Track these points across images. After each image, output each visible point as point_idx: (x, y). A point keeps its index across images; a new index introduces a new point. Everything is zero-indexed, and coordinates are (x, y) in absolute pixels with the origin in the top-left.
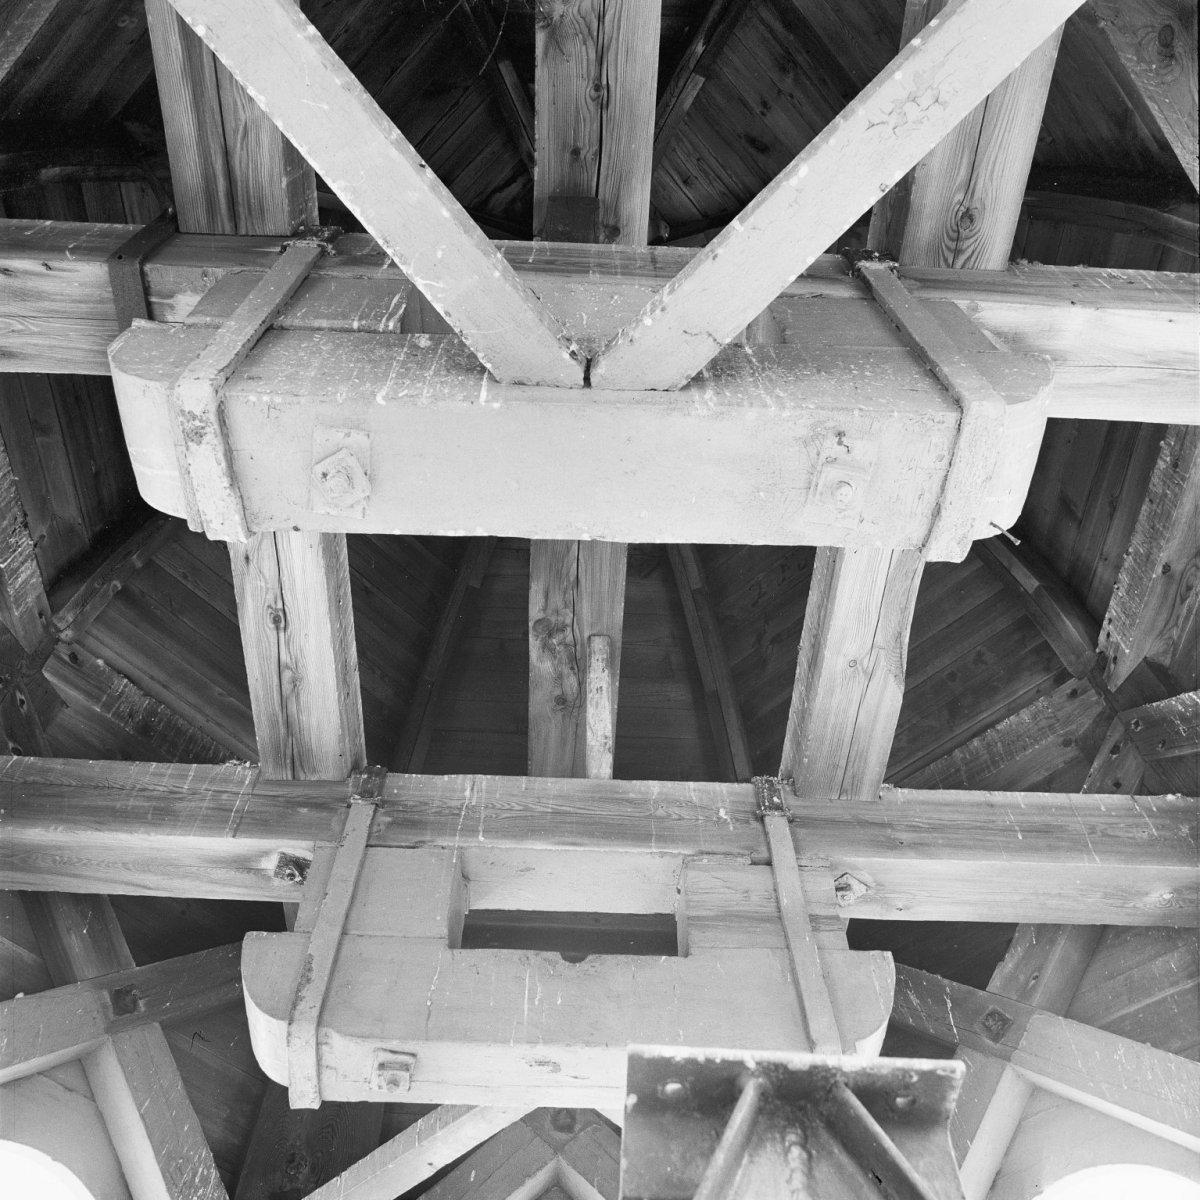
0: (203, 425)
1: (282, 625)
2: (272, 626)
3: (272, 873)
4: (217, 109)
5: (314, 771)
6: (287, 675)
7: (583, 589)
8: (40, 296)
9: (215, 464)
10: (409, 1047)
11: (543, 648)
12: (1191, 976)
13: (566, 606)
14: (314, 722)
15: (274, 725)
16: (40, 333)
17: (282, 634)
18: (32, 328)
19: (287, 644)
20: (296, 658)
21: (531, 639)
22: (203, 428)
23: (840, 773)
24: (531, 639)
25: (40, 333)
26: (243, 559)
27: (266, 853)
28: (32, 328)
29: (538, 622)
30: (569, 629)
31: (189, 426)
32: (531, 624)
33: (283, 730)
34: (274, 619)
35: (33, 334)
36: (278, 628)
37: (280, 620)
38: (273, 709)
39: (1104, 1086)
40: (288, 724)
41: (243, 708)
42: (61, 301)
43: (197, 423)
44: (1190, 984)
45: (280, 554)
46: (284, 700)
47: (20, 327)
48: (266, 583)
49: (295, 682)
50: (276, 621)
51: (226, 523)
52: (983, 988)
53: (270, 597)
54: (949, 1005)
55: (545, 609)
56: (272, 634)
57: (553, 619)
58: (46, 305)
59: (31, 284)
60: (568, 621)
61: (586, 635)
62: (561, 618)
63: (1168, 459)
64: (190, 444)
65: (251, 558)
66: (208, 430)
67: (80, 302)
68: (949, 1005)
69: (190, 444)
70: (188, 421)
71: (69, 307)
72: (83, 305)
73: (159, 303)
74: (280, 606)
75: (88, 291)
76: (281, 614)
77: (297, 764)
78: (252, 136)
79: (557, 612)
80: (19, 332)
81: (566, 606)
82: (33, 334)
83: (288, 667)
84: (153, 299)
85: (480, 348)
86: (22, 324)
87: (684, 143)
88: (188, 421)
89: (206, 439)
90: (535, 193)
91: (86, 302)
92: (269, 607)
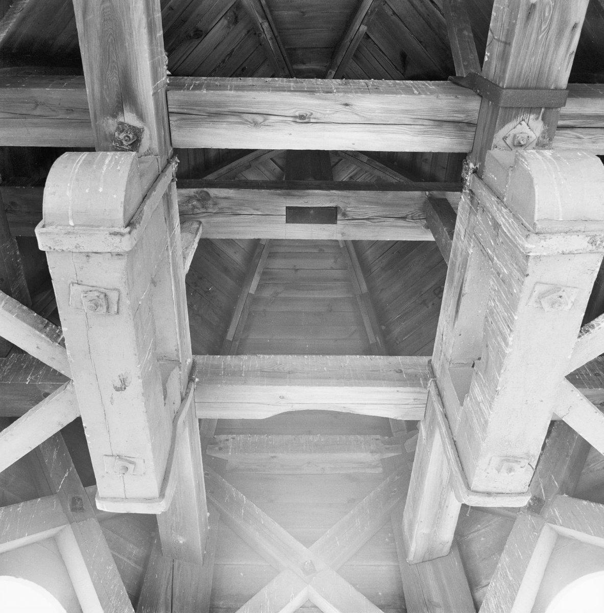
0: (597, 244)
1: (298, 120)
2: (297, 114)
3: (121, 119)
4: (591, 126)
5: (179, 127)
6: (259, 119)
7: (232, 218)
8: (558, 45)
9: (576, 249)
10: (124, 309)
11: (189, 197)
12: (136, 562)
13: (219, 209)
14: (222, 131)
15: (217, 104)
16: (537, 39)
17: (291, 119)
18: (541, 36)
19: (282, 121)
20: (273, 126)
21: (195, 190)
22: (595, 245)
23: (213, 401)
24: (194, 189)
25: (537, 39)
26: (347, 102)
27: (141, 116)
28: (541, 36)
29: (208, 194)
30: (204, 210)
31: (598, 238)
32: (205, 189)
33: (214, 110)
34: (303, 116)
35: (538, 35)
36: (295, 117)
37: (303, 119)
38: (230, 106)
39: (95, 573)
40: (218, 114)
41: (422, 244)
42: (552, 57)
43: (599, 242)
44: (133, 565)
45: (349, 125)
46: (239, 114)
47: (543, 29)
48: (328, 114)
49: (256, 124)
50: (302, 117)
51: (543, 249)
52: (84, 486)
53: (318, 115)
54: (66, 475)
55: (217, 197)
56: (291, 112)
57: (210, 202)
58: (553, 45)
59: (565, 42)
60: (210, 210)
61: (202, 220)
62: (211, 206)
63: (315, 441)
64: (589, 238)
65: (347, 107)
66: (594, 247)
67: (550, 68)
68: (66, 475)
69: (589, 238)
70: (601, 239)
71: (548, 61)
72: (547, 69)
73: (540, 112)
74: (312, 120)
75: (555, 73)
76: (306, 120)
77: (184, 116)
78: (577, 141)
79: (215, 204)
80: (541, 27)
81: (219, 209)
82: (538, 35)
83: (265, 120)
84: (520, 86)
85: (582, 340)
86: (544, 30)
87: (370, 177)
88: (601, 239)
89: (590, 246)
90: (449, 192)
91: (549, 71)
92: (312, 114)
